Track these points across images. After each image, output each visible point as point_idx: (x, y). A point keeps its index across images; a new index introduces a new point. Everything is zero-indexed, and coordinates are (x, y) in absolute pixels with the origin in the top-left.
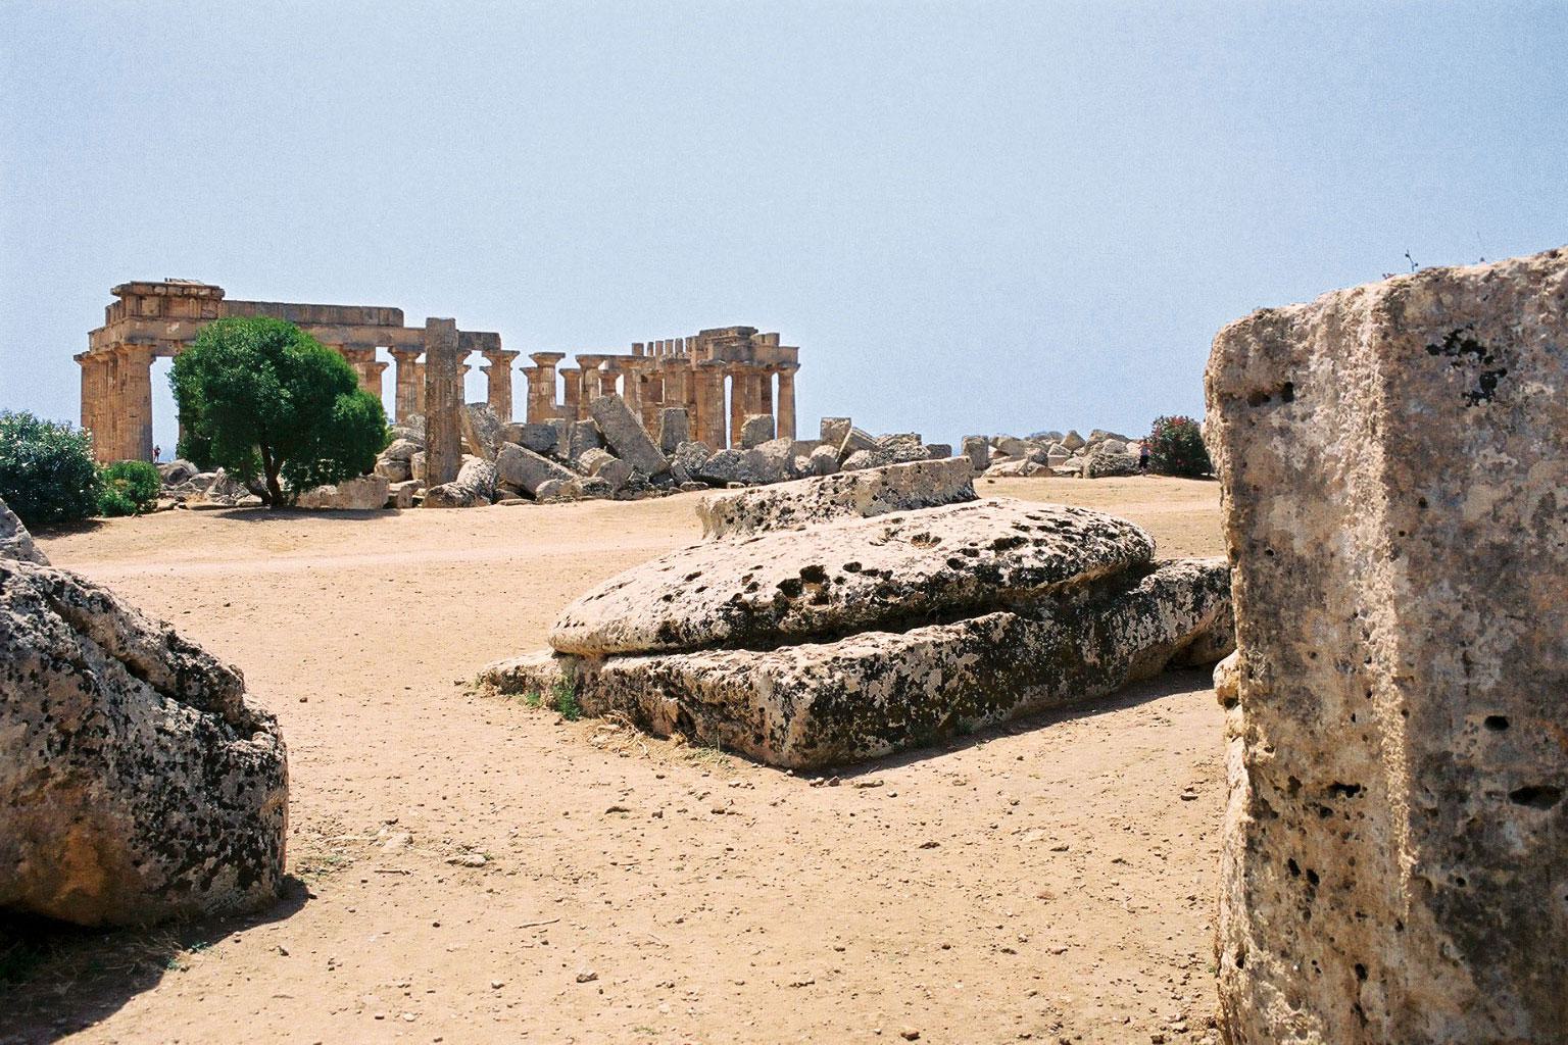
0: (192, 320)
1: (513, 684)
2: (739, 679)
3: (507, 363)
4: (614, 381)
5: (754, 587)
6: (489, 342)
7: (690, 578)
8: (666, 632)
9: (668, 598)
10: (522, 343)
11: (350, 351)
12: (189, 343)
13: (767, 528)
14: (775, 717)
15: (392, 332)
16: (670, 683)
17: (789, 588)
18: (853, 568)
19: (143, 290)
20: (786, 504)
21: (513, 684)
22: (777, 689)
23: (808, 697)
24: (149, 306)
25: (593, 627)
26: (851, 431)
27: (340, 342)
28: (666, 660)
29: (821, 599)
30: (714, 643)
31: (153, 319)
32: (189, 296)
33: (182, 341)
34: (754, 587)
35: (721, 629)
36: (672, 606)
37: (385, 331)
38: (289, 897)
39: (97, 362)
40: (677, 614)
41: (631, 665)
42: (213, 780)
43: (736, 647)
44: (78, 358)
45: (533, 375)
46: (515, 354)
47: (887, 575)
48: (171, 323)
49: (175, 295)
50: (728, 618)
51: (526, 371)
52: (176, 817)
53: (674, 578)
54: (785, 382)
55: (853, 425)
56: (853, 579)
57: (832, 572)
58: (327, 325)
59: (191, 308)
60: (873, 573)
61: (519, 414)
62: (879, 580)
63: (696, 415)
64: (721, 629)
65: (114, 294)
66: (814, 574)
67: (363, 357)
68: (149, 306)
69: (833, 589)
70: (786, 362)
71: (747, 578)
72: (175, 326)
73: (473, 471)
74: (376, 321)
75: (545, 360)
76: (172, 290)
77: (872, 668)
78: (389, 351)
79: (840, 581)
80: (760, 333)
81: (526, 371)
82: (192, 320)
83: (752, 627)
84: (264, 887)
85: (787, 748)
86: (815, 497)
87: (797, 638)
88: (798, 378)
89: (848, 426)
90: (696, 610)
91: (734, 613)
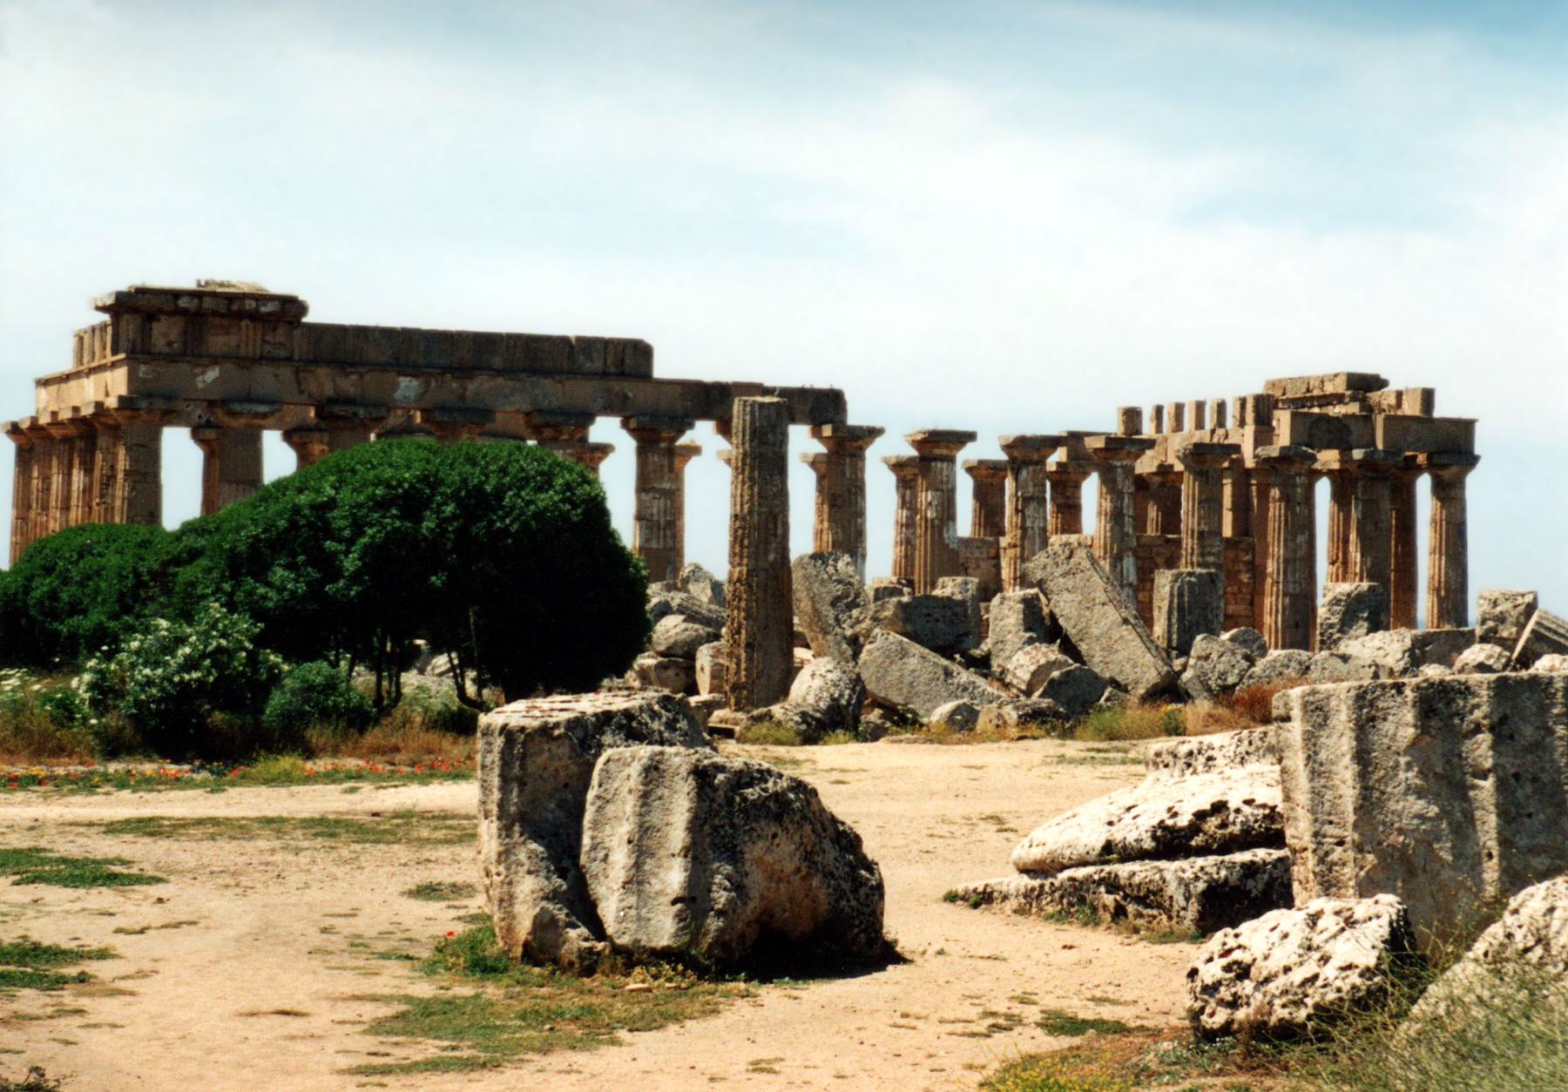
0: (244, 362)
1: (983, 899)
2: (1157, 877)
3: (858, 456)
4: (1077, 486)
5: (1175, 815)
6: (822, 406)
7: (1129, 809)
8: (1108, 847)
9: (1111, 823)
10: (892, 412)
11: (547, 425)
12: (237, 407)
13: (1194, 772)
14: (1180, 900)
15: (631, 389)
16: (1112, 885)
17: (1201, 816)
18: (1249, 802)
19: (156, 302)
20: (1210, 753)
21: (983, 899)
22: (1181, 880)
23: (1201, 886)
24: (165, 333)
25: (1050, 847)
26: (1534, 618)
27: (526, 407)
28: (1107, 868)
29: (1224, 825)
30: (1142, 855)
31: (172, 358)
32: (242, 315)
33: (224, 402)
34: (1175, 815)
35: (1148, 844)
36: (1113, 829)
37: (616, 386)
38: (883, 955)
39: (51, 438)
40: (1118, 834)
41: (1080, 873)
42: (855, 890)
43: (1158, 859)
44: (14, 430)
45: (909, 472)
46: (873, 433)
47: (1273, 808)
48: (206, 366)
49: (215, 313)
50: (1154, 837)
51: (898, 466)
52: (843, 903)
53: (1116, 810)
54: (1450, 493)
55: (1542, 605)
56: (1247, 810)
57: (1232, 805)
58: (499, 372)
59: (243, 338)
60: (1264, 806)
61: (880, 561)
62: (1267, 811)
63: (1252, 562)
64: (1148, 844)
65: (98, 308)
66: (1219, 807)
67: (571, 435)
68: (165, 333)
69: (1231, 818)
70: (1450, 448)
71: (1170, 809)
72: (212, 374)
73: (818, 682)
74: (598, 365)
75: (937, 448)
76: (208, 303)
77: (1250, 869)
78: (625, 425)
79: (1238, 811)
80: (1393, 386)
81: (898, 466)
82: (244, 362)
83: (1171, 842)
84: (877, 950)
85: (1187, 922)
86: (1233, 748)
87: (1203, 851)
88: (1475, 483)
89: (1531, 608)
90: (1136, 831)
91: (1159, 833)
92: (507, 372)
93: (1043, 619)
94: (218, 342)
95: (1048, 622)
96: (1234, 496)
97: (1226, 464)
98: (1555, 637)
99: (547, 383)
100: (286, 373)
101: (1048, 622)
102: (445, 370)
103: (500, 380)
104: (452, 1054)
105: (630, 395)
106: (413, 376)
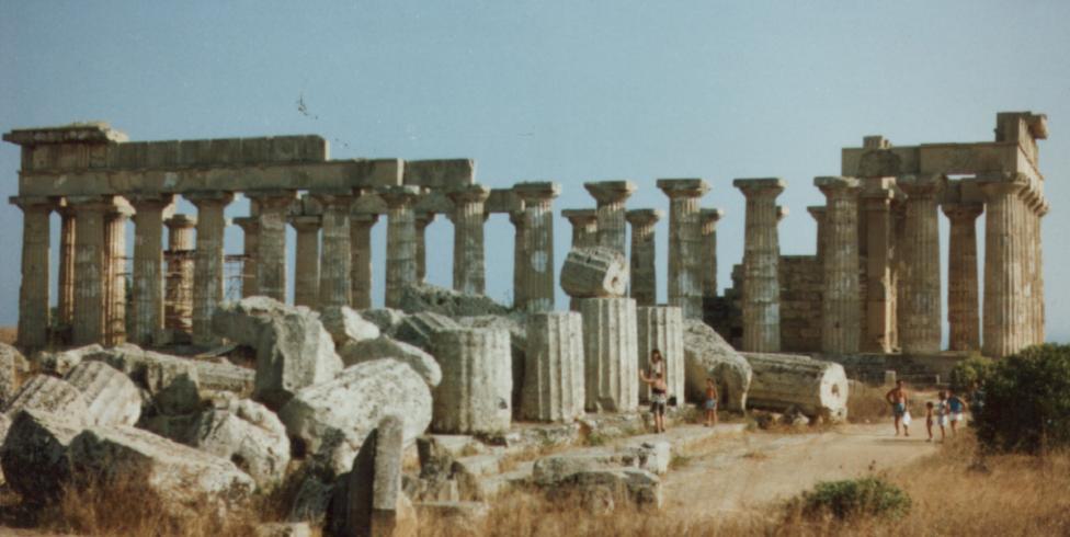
58: (224, 165)
72: (62, 180)
92: (231, 165)
93: (270, 355)
94: (67, 160)
95: (274, 359)
96: (160, 239)
97: (428, 190)
98: (600, 322)
99: (255, 171)
100: (103, 177)
101: (274, 359)
102: (192, 166)
103: (226, 171)
104: (649, 321)
105: (308, 173)
106: (173, 171)
